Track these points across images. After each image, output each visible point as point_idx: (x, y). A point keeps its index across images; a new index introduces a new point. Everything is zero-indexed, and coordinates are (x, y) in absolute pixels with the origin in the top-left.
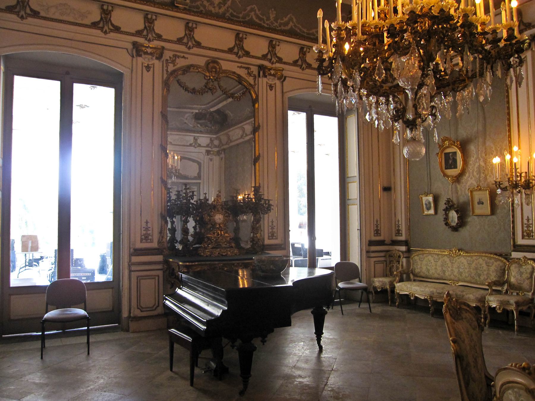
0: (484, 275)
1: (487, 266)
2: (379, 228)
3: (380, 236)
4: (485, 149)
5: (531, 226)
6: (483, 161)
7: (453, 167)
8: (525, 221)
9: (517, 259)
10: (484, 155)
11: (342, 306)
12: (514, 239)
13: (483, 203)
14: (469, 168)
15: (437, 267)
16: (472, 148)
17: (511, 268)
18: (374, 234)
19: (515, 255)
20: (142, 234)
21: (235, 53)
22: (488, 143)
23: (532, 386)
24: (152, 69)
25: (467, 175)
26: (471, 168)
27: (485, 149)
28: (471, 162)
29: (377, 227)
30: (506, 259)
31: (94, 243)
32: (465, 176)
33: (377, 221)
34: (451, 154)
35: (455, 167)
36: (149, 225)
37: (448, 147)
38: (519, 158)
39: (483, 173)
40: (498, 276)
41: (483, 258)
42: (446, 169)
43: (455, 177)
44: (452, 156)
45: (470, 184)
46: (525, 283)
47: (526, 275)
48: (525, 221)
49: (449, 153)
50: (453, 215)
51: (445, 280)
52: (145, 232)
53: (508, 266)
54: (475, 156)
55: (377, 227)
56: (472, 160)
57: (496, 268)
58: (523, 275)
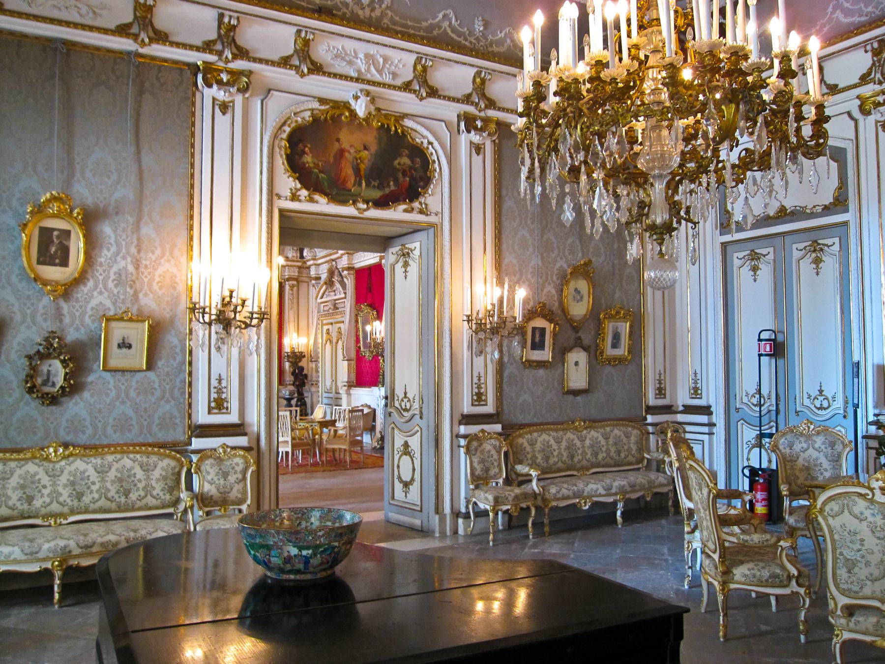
0: (236, 472)
1: (144, 471)
2: (662, 386)
3: (665, 398)
4: (139, 239)
5: (224, 390)
6: (132, 262)
7: (57, 261)
8: (214, 383)
9: (211, 449)
10: (133, 250)
11: (130, 629)
12: (190, 416)
13: (130, 347)
14: (97, 271)
15: (610, 447)
16: (106, 229)
17: (202, 468)
18: (656, 394)
19: (197, 443)
20: (212, 399)
21: (217, 51)
22: (146, 230)
23: (884, 544)
24: (230, 109)
25: (91, 284)
26: (101, 271)
27: (139, 239)
28: (103, 260)
29: (479, 387)
30: (178, 452)
31: (392, 574)
32: (85, 285)
33: (660, 374)
34: (55, 233)
35: (64, 263)
36: (224, 384)
37: (53, 216)
38: (506, 286)
39: (131, 287)
40: (169, 487)
41: (131, 456)
42: (39, 263)
43: (65, 285)
44: (58, 237)
45: (97, 305)
46: (235, 490)
47: (235, 477)
48: (214, 383)
49: (53, 230)
50: (57, 370)
51: (29, 517)
52: (216, 396)
53: (197, 465)
54: (113, 249)
55: (479, 387)
56: (104, 256)
57: (164, 473)
58: (229, 477)
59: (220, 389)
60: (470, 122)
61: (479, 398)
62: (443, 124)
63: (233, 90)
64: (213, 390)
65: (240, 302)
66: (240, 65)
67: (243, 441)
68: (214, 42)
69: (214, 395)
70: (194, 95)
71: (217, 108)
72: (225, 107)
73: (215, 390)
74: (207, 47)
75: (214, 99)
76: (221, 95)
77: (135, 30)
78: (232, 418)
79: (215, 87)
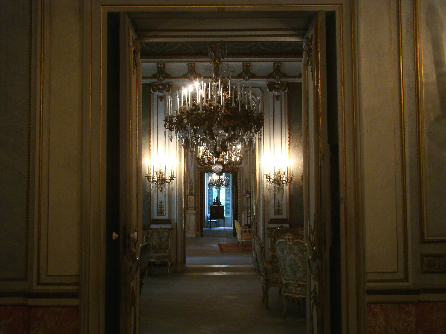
12: (150, 216)
19: (152, 226)
20: (276, 209)
24: (280, 98)
48: (159, 204)
52: (277, 208)
59: (279, 206)
60: (271, 87)
61: (278, 211)
62: (259, 89)
63: (281, 91)
64: (276, 206)
65: (283, 173)
66: (166, 81)
67: (169, 226)
68: (156, 74)
69: (277, 208)
70: (150, 96)
71: (159, 99)
72: (278, 97)
73: (277, 206)
74: (154, 76)
75: (158, 96)
76: (276, 93)
77: (244, 75)
78: (166, 217)
79: (157, 92)
